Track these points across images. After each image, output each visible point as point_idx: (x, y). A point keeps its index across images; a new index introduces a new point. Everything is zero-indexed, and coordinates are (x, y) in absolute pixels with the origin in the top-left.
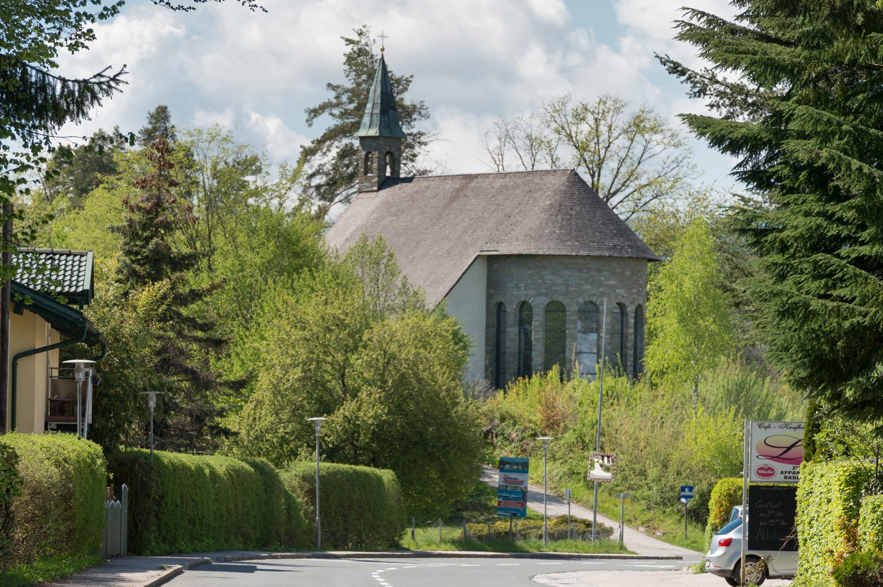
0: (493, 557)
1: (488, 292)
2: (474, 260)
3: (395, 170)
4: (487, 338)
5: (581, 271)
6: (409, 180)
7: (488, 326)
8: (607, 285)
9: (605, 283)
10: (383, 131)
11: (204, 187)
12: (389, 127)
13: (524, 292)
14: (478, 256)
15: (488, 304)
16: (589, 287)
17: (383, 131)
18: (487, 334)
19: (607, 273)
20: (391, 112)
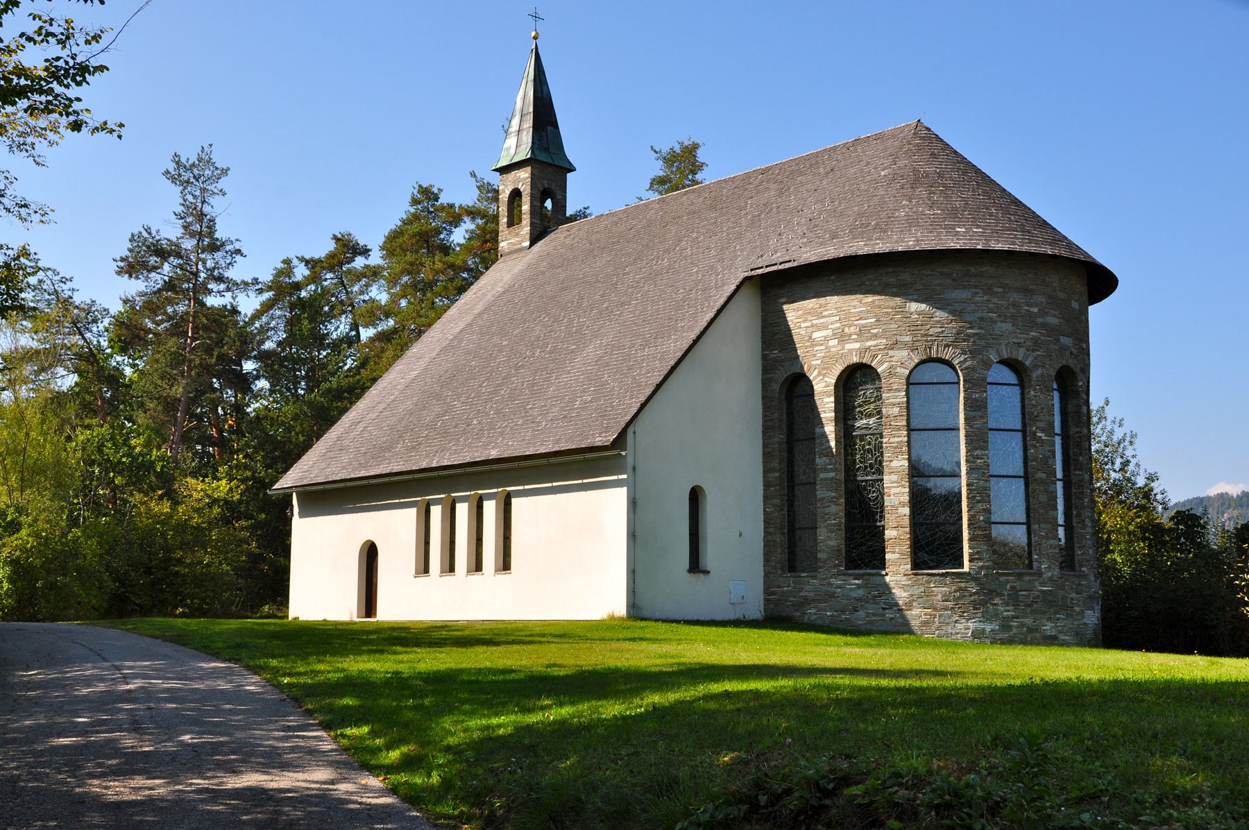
0: (918, 673)
1: (764, 357)
2: (739, 287)
3: (560, 205)
4: (767, 456)
5: (989, 291)
6: (573, 218)
7: (767, 430)
8: (1044, 325)
9: (1040, 320)
10: (537, 153)
11: (332, 782)
12: (547, 150)
13: (857, 345)
14: (746, 279)
15: (766, 384)
16: (1008, 327)
17: (537, 153)
18: (765, 446)
19: (1042, 299)
20: (549, 128)
